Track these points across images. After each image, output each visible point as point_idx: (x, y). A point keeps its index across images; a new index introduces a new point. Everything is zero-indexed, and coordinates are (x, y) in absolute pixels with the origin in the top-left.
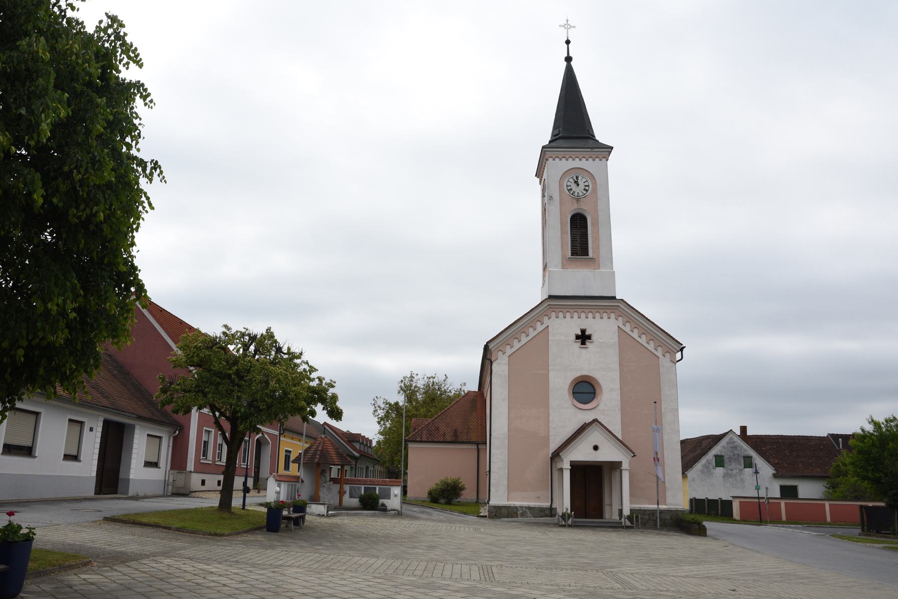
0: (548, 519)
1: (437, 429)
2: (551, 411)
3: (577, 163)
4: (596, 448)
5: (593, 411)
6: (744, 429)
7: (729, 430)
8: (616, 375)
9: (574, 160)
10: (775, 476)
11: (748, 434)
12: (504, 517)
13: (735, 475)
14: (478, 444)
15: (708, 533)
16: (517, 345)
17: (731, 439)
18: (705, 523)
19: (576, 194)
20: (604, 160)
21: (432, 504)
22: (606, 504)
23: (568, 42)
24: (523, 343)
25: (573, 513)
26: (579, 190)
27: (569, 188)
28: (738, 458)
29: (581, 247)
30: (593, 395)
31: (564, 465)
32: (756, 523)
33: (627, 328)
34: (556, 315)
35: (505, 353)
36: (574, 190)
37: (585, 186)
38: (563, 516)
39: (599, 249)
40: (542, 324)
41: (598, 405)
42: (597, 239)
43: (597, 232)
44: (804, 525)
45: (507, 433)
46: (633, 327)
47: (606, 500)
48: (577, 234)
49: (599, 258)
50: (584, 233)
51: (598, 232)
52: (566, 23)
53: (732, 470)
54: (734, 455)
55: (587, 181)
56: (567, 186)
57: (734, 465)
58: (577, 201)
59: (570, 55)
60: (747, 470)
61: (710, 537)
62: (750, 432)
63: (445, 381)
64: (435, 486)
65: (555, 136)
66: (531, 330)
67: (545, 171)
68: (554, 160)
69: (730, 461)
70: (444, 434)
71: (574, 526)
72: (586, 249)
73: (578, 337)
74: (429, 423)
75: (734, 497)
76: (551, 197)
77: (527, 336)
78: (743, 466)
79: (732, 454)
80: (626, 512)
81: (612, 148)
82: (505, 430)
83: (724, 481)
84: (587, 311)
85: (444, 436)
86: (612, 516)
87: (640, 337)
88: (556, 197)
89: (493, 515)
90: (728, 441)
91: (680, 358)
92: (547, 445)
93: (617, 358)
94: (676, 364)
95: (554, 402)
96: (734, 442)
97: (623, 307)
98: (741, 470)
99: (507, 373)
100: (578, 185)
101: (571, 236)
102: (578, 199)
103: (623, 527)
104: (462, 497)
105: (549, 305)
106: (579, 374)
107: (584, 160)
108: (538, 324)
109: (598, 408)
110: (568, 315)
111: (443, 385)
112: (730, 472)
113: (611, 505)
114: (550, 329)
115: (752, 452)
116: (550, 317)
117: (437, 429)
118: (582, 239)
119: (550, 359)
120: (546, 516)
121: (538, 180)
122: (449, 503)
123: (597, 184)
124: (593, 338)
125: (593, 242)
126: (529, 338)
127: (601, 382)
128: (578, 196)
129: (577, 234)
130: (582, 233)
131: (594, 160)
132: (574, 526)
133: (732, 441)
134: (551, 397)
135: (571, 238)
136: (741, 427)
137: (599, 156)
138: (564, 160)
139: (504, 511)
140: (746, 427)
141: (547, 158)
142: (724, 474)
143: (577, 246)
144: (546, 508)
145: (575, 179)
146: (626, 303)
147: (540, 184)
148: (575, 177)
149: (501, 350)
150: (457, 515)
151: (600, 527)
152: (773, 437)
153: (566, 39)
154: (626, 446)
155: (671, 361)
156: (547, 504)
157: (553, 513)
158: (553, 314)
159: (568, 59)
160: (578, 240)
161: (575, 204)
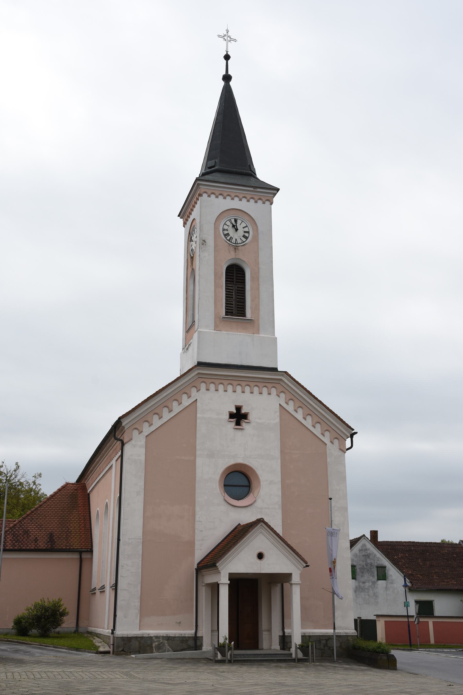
0: (189, 654)
1: (26, 532)
2: (197, 509)
3: (236, 204)
4: (260, 556)
5: (249, 508)
6: (374, 534)
7: (362, 535)
8: (277, 465)
9: (233, 199)
10: (412, 590)
11: (379, 540)
12: (135, 653)
13: (368, 589)
14: (81, 553)
15: (398, 665)
16: (157, 422)
17: (364, 545)
18: (393, 652)
19: (234, 241)
20: (267, 203)
21: (22, 638)
22: (263, 629)
23: (227, 57)
24: (165, 419)
25: (233, 643)
26: (237, 236)
27: (226, 232)
28: (370, 569)
29: (238, 305)
30: (246, 489)
31: (222, 578)
32: (405, 648)
33: (290, 408)
34: (206, 386)
35: (142, 432)
36: (231, 235)
37: (245, 232)
38: (221, 648)
39: (259, 310)
40: (189, 397)
41: (255, 501)
42: (256, 298)
43: (257, 289)
44: (458, 648)
45: (142, 538)
46: (297, 406)
47: (264, 625)
48: (232, 290)
49: (258, 320)
50: (241, 289)
51: (258, 289)
52: (225, 33)
53: (364, 583)
54: (367, 565)
55: (247, 226)
56: (224, 230)
57: (366, 576)
58: (235, 249)
59: (230, 73)
60: (380, 582)
61: (399, 670)
62: (381, 538)
63: (15, 471)
64: (26, 612)
65: (209, 168)
66: (175, 404)
67: (197, 206)
68: (209, 196)
69: (363, 572)
70: (36, 540)
71: (235, 661)
72: (243, 308)
73: (232, 416)
74: (15, 525)
75: (378, 616)
76: (204, 241)
77: (170, 411)
78: (376, 577)
79: (364, 563)
80: (297, 640)
81: (278, 190)
82: (139, 533)
83: (356, 596)
84: (243, 384)
85: (36, 542)
86: (271, 646)
87: (305, 419)
88: (211, 242)
89: (121, 649)
90: (361, 549)
91: (350, 446)
92: (192, 553)
93: (277, 444)
94: (345, 453)
95: (200, 498)
96: (366, 550)
97: (286, 381)
98: (374, 583)
99: (143, 458)
100: (237, 230)
101: (226, 291)
102: (236, 247)
103: (294, 660)
104: (64, 625)
105: (199, 374)
106: (232, 462)
107: (244, 200)
108: (185, 397)
109: (255, 504)
110: (221, 387)
111: (13, 476)
112: (362, 585)
113: (270, 630)
114: (199, 404)
115: (385, 562)
116: (199, 389)
117: (27, 532)
118: (238, 295)
119: (198, 442)
120: (189, 648)
121: (181, 221)
122: (45, 634)
123: (259, 232)
124: (250, 417)
125: (252, 301)
126: (172, 414)
127: (259, 472)
128: (235, 243)
129: (232, 290)
130: (239, 289)
131: (256, 202)
132: (233, 661)
133: (364, 548)
134: (197, 491)
135: (226, 294)
136: (371, 531)
137: (263, 198)
138: (221, 197)
139: (135, 644)
140: (377, 531)
141: (201, 193)
142: (356, 587)
143: (232, 304)
144: (189, 637)
145: (233, 222)
146: (290, 376)
147: (184, 226)
148: (233, 221)
149: (136, 429)
150: (66, 653)
151: (266, 661)
152: (404, 544)
153: (225, 53)
154: (297, 554)
155: (340, 449)
156: (190, 632)
157: (198, 643)
158: (203, 386)
159: (227, 78)
160: (234, 296)
161: (233, 253)
